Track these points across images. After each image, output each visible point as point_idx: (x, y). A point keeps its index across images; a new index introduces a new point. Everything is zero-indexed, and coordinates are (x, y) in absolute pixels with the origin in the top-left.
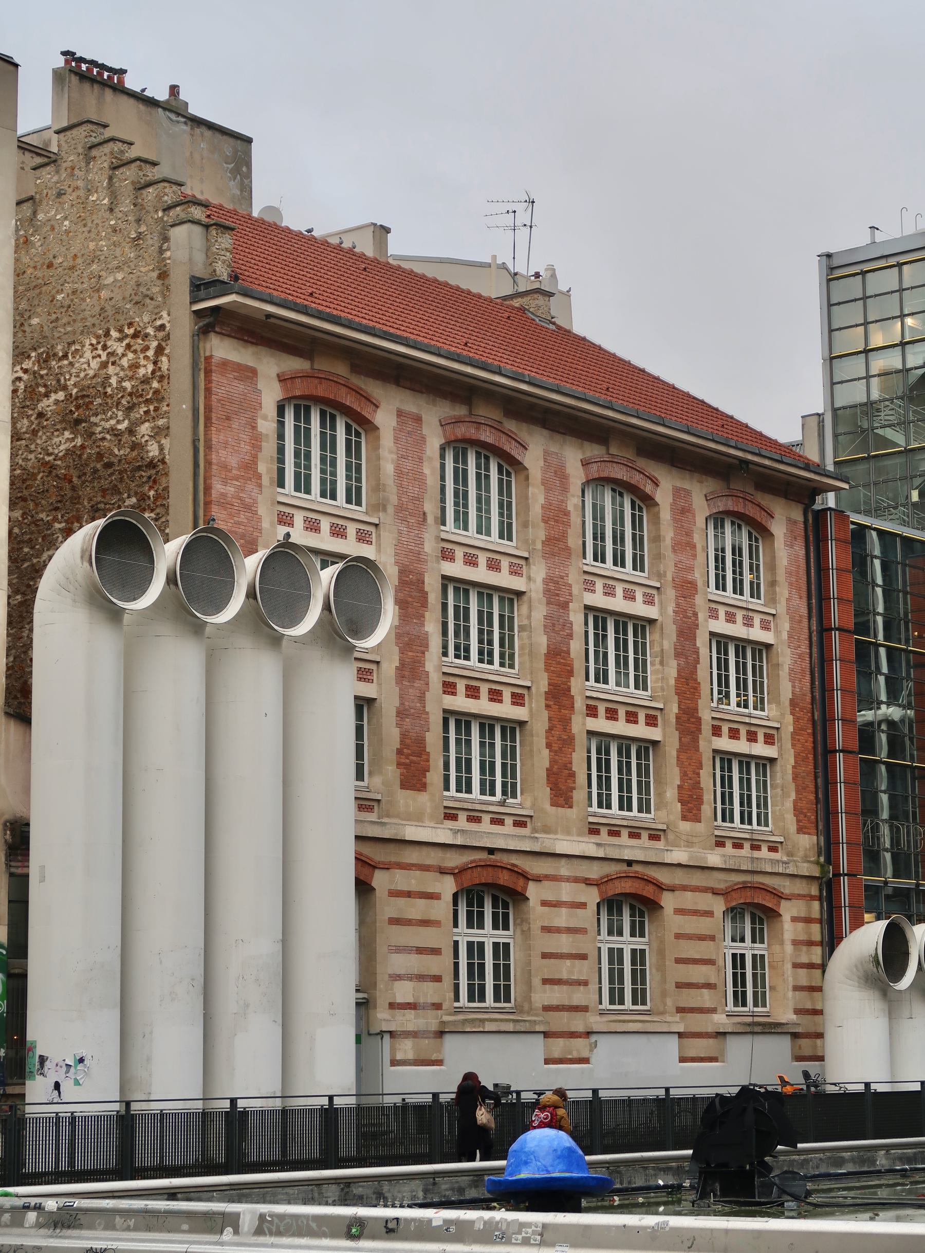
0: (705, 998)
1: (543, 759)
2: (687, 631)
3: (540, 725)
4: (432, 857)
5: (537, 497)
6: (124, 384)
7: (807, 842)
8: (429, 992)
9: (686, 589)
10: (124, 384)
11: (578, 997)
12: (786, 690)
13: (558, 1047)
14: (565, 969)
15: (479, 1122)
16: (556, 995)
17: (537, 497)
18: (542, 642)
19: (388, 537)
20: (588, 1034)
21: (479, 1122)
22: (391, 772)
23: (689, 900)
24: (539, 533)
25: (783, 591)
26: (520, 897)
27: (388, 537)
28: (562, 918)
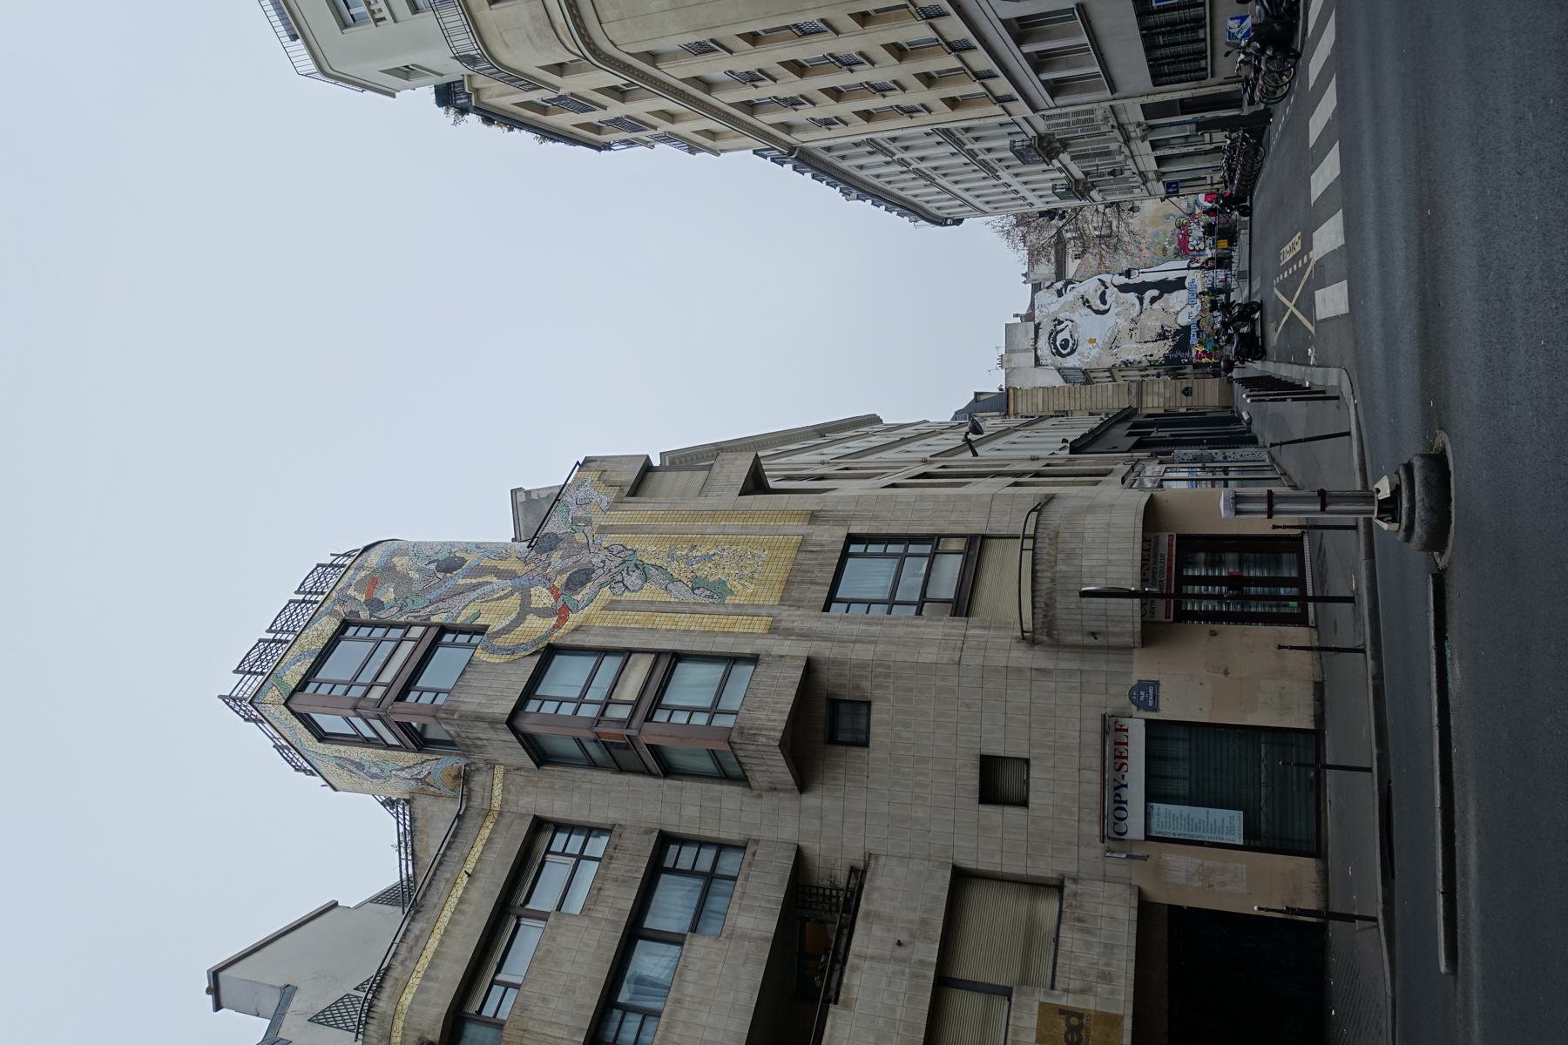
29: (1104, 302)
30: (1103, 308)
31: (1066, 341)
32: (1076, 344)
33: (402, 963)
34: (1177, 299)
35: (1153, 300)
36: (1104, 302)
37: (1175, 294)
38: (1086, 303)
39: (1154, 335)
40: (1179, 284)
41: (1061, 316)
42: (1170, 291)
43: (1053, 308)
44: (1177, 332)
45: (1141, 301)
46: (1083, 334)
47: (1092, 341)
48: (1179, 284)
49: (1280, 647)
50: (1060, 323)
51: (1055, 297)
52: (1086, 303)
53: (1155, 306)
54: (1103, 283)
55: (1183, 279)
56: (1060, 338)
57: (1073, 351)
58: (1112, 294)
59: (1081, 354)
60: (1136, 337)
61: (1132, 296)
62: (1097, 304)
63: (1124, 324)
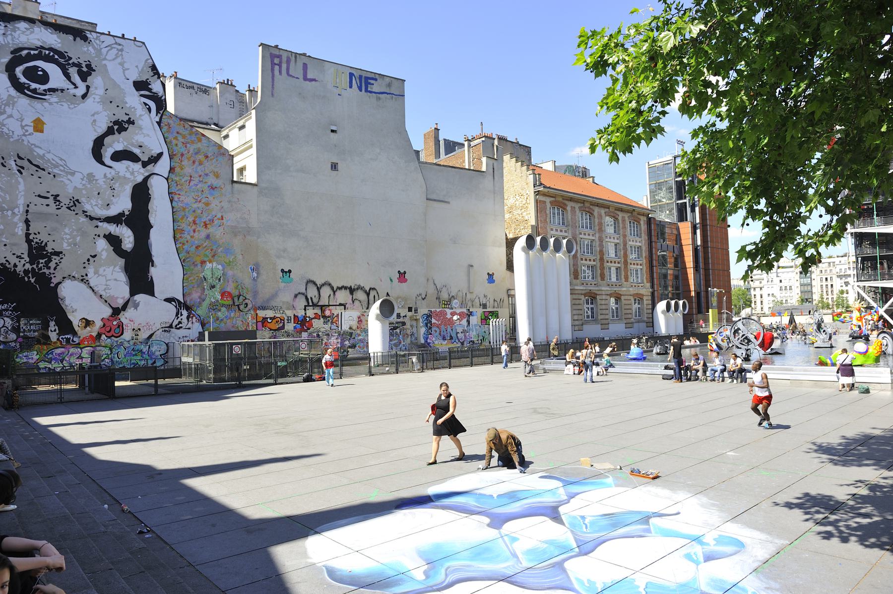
0: (630, 316)
1: (599, 272)
2: (625, 245)
3: (598, 265)
4: (580, 292)
5: (597, 221)
6: (807, 254)
7: (649, 285)
8: (580, 317)
9: (625, 236)
10: (807, 254)
11: (607, 317)
12: (644, 255)
13: (603, 326)
14: (604, 312)
15: (124, 260)
16: (602, 317)
17: (597, 221)
18: (598, 249)
19: (570, 232)
20: (27, 222)
21: (124, 260)
22: (599, 278)
23: (626, 297)
24: (597, 228)
25: (643, 235)
26: (595, 298)
27: (570, 232)
28: (603, 302)
29: (118, 156)
30: (107, 153)
31: (44, 78)
32: (35, 95)
33: (605, 326)
34: (114, 280)
35: (114, 241)
36: (118, 156)
37: (122, 277)
38: (119, 126)
39: (43, 237)
40: (140, 279)
41: (96, 80)
42: (127, 270)
43: (113, 69)
44: (44, 280)
45: (115, 220)
46: (51, 110)
47: (39, 126)
48: (140, 279)
49: (678, 513)
50: (84, 76)
51: (134, 76)
52: (119, 126)
53: (102, 244)
54: (155, 159)
55: (149, 289)
56: (53, 70)
57: (19, 87)
58: (134, 172)
59: (10, 102)
60: (39, 206)
61: (124, 204)
62: (116, 143)
63: (69, 187)
